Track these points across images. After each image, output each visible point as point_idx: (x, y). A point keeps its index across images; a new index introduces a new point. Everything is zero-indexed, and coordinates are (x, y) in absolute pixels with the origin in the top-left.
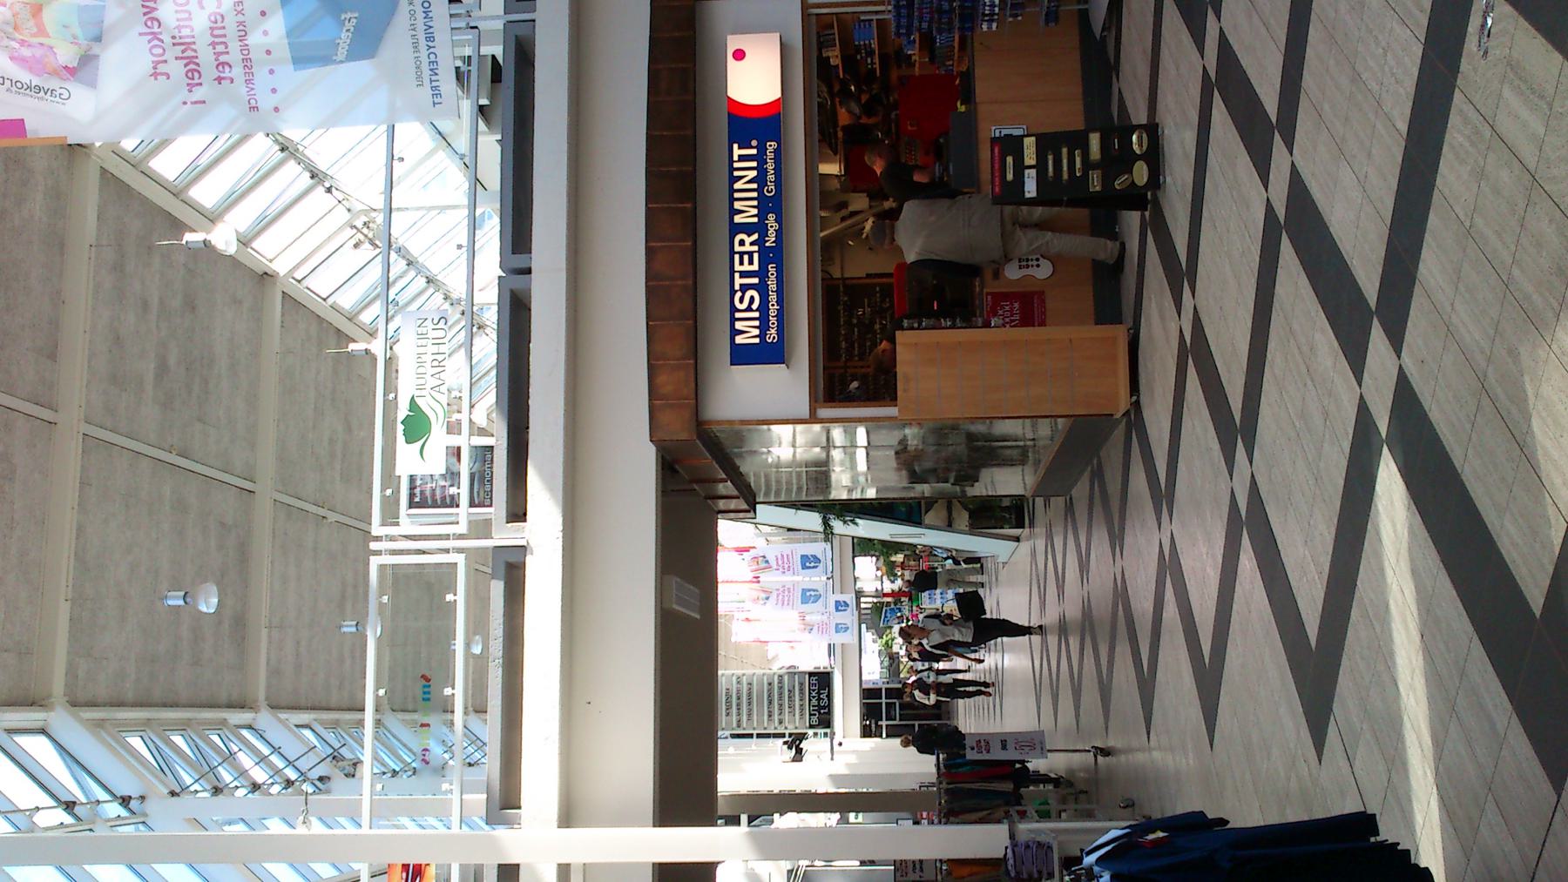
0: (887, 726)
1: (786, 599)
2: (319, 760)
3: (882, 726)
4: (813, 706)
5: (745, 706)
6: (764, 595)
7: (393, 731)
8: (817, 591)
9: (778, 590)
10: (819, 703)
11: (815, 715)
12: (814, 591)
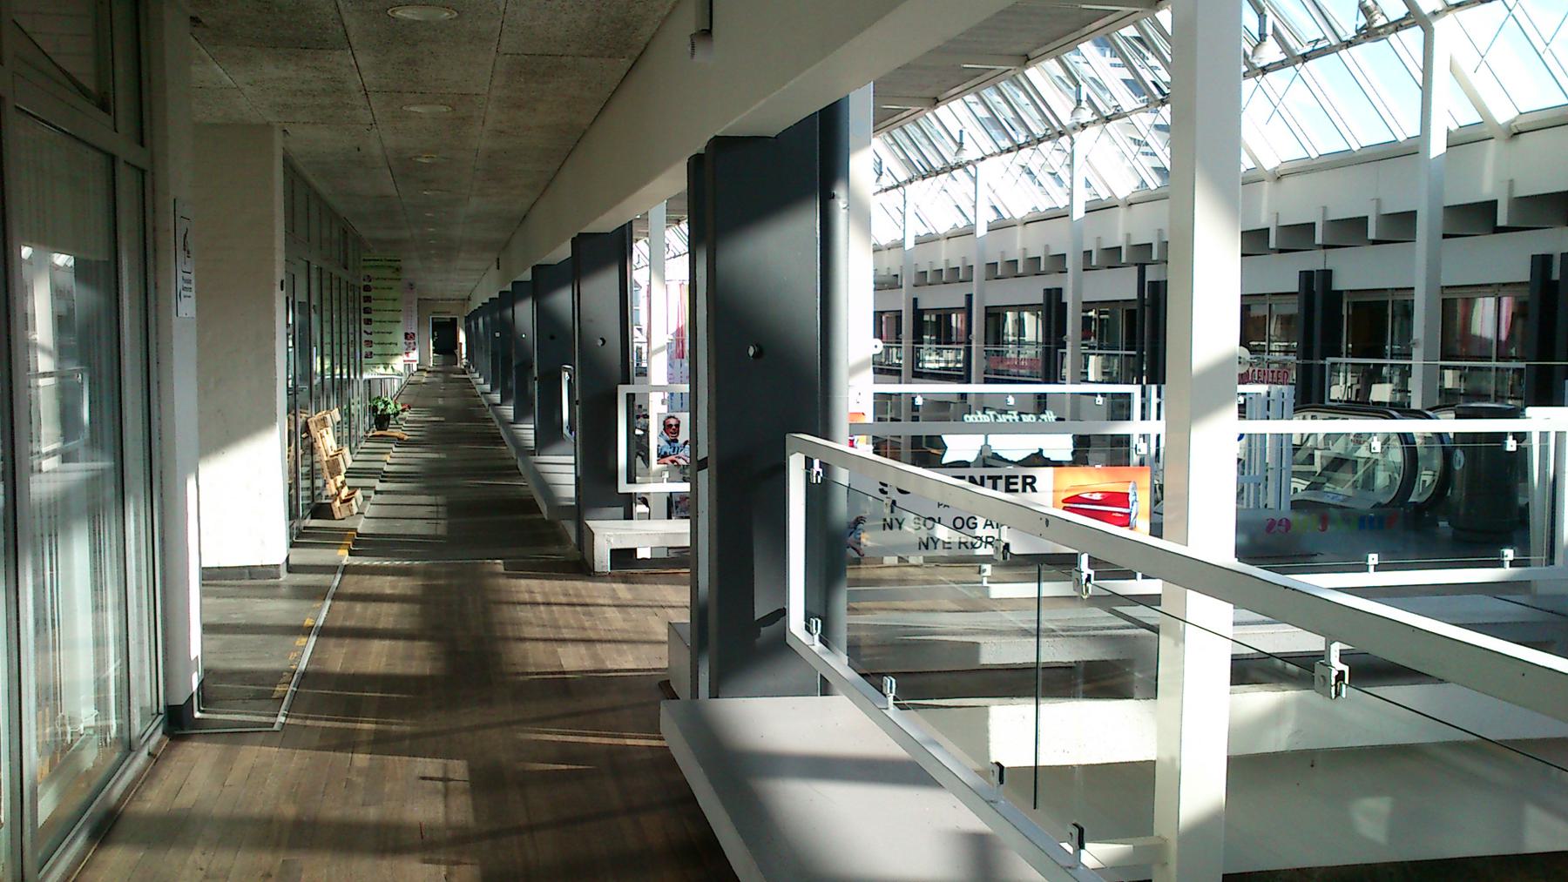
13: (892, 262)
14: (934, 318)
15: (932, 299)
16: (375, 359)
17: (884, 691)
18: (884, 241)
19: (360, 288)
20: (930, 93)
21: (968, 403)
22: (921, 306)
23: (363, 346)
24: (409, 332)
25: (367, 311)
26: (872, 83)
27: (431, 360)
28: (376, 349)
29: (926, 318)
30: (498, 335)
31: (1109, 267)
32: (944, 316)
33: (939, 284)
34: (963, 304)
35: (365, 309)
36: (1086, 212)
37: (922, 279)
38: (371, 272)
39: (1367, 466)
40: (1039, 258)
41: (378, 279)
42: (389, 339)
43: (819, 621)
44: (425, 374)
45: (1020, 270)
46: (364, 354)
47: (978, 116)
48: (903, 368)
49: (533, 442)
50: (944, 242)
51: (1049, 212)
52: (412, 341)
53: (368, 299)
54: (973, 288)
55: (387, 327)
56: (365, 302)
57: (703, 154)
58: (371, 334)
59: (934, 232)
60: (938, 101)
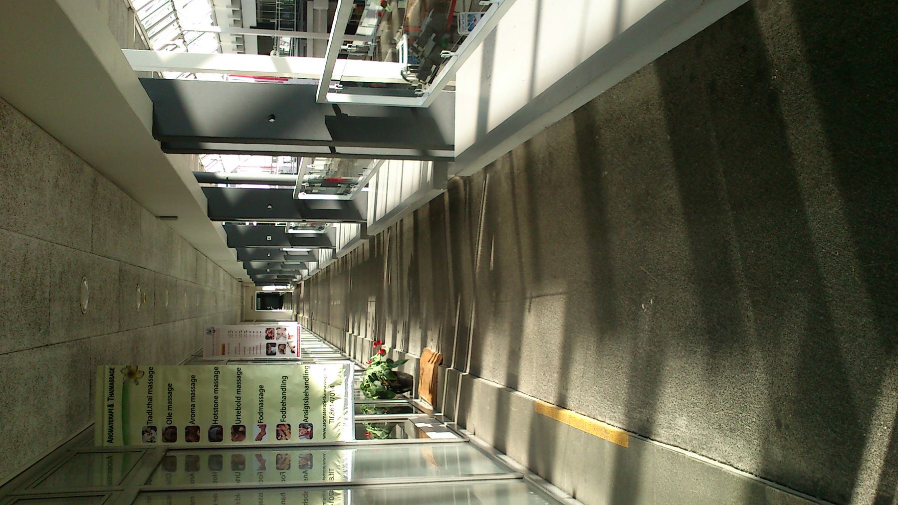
13: (229, 42)
16: (314, 419)
17: (449, 57)
18: (215, 44)
19: (169, 450)
20: (125, 10)
23: (289, 442)
24: (265, 335)
25: (216, 434)
26: (122, 49)
27: (287, 311)
28: (295, 418)
30: (269, 238)
33: (242, 12)
35: (211, 439)
36: (217, 25)
37: (239, 22)
38: (138, 424)
39: (261, 471)
41: (150, 413)
42: (273, 392)
43: (443, 52)
44: (301, 315)
46: (305, 441)
49: (330, 250)
50: (216, 8)
51: (213, 18)
52: (276, 331)
53: (192, 433)
55: (250, 395)
56: (197, 439)
57: (161, 143)
58: (263, 427)
59: (210, 14)
60: (130, 7)
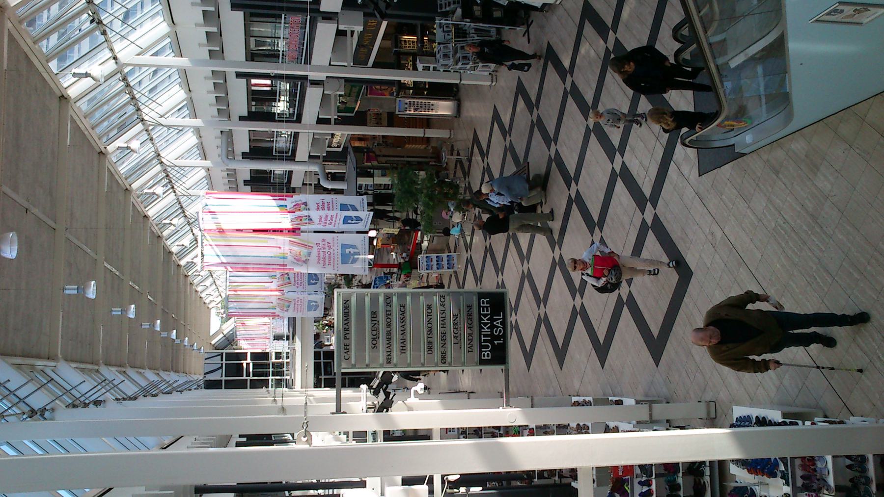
0: (325, 379)
1: (299, 308)
2: (36, 389)
3: (321, 379)
4: (485, 336)
5: (475, 312)
6: (287, 304)
7: (131, 376)
8: (317, 303)
9: (294, 300)
10: (492, 331)
11: (487, 347)
12: (315, 302)
14: (254, 103)
15: (240, 104)
21: (324, 79)
22: (245, 114)
29: (253, 109)
31: (219, 17)
32: (255, 96)
34: (244, 81)
37: (224, 113)
40: (214, 83)
45: (215, 29)
47: (89, 50)
48: (294, 131)
54: (231, 71)
